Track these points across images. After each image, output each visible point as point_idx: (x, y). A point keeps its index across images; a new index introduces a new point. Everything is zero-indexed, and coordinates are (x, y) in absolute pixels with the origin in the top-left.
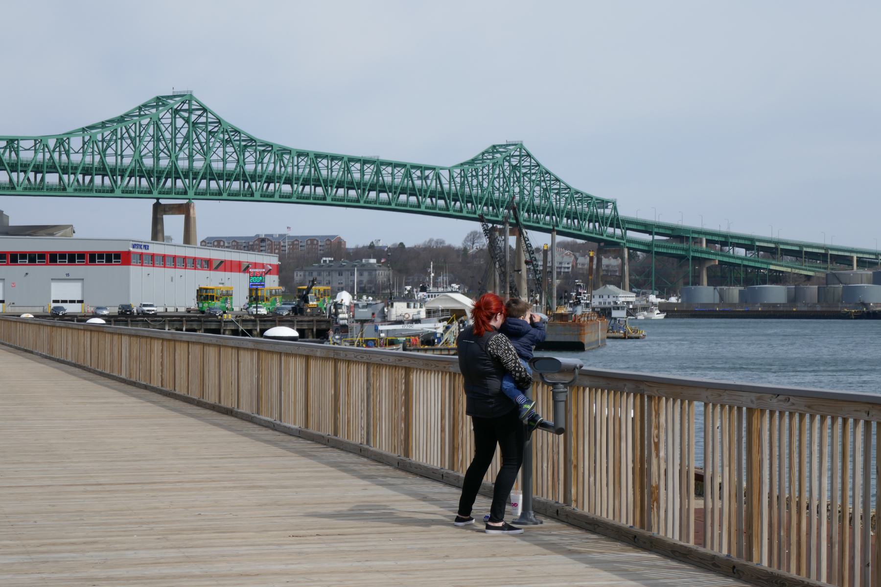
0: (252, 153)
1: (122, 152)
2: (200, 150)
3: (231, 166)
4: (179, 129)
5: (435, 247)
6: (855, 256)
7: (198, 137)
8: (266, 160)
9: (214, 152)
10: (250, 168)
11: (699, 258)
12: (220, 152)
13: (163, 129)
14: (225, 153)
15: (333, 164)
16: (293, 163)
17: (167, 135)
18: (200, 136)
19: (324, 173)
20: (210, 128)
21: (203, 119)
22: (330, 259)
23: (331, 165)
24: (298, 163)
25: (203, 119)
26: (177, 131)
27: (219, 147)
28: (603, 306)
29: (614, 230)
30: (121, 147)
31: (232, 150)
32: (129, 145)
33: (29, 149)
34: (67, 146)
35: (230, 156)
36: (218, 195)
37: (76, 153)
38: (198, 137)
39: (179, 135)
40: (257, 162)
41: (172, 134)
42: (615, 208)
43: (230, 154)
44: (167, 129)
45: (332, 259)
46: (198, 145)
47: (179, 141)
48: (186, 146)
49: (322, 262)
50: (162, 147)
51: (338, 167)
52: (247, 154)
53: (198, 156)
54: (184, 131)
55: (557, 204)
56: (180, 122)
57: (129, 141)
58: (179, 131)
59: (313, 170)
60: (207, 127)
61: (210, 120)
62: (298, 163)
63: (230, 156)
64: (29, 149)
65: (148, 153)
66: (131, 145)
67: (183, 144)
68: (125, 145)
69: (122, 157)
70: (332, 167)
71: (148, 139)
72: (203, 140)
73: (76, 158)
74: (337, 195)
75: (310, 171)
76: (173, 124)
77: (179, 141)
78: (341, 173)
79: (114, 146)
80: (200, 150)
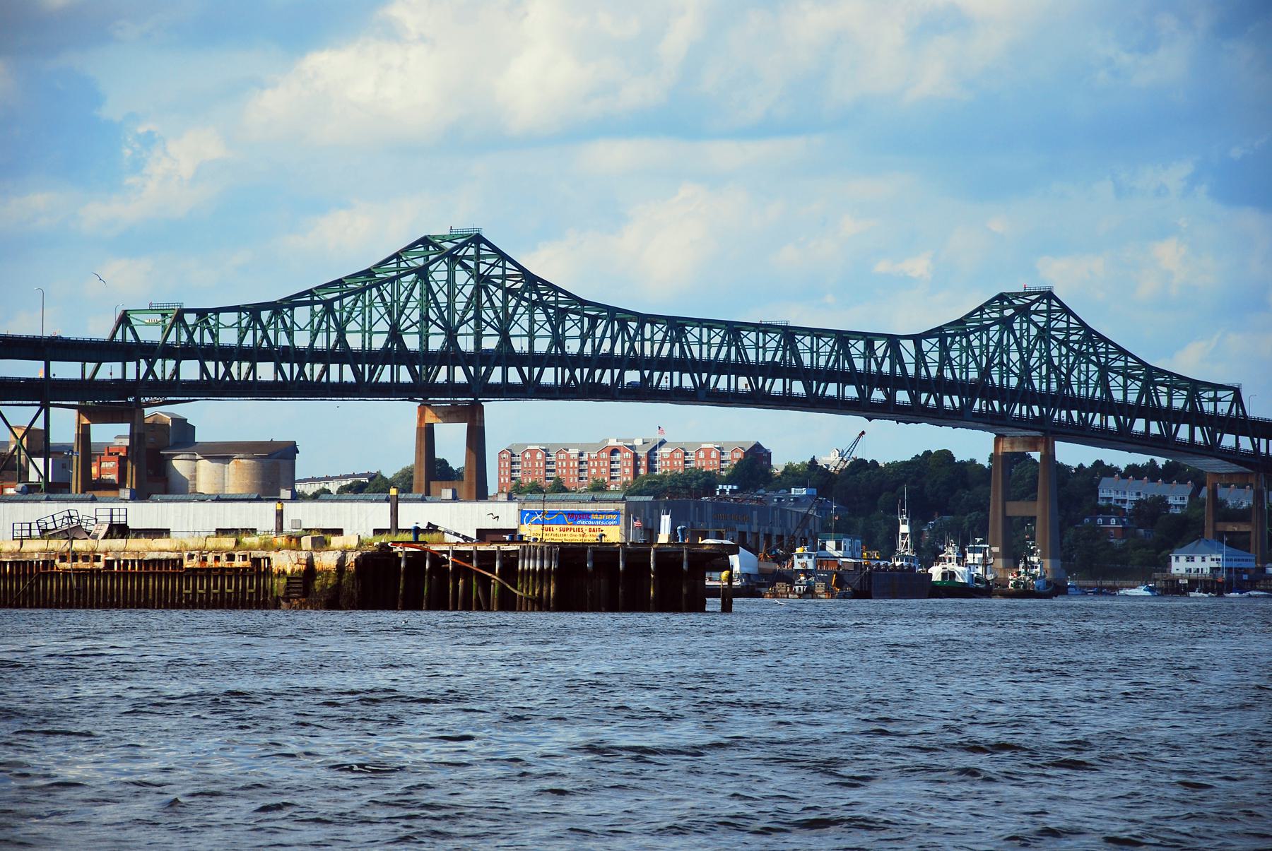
0: (576, 322)
1: (371, 326)
2: (492, 320)
3: (542, 346)
4: (460, 287)
5: (681, 471)
6: (73, 495)
7: (490, 300)
8: (599, 332)
9: (516, 322)
10: (572, 347)
11: (641, 495)
12: (524, 321)
13: (435, 289)
14: (532, 321)
15: (768, 339)
16: (643, 335)
17: (442, 298)
18: (494, 297)
19: (806, 359)
20: (508, 284)
21: (498, 271)
22: (730, 487)
23: (818, 345)
24: (709, 341)
25: (498, 271)
26: (457, 291)
27: (524, 313)
28: (1193, 575)
29: (1237, 440)
30: (370, 317)
31: (543, 317)
32: (382, 317)
33: (231, 327)
34: (288, 321)
35: (542, 327)
36: (531, 390)
37: (301, 330)
38: (490, 300)
39: (460, 298)
40: (583, 338)
41: (448, 296)
42: (1238, 399)
43: (541, 323)
44: (441, 289)
45: (735, 487)
46: (491, 313)
47: (460, 307)
48: (471, 314)
49: (718, 493)
50: (433, 316)
51: (829, 349)
52: (568, 324)
53: (489, 330)
54: (468, 290)
55: (961, 374)
56: (461, 276)
57: (383, 310)
58: (460, 291)
59: (733, 349)
60: (504, 282)
61: (508, 272)
62: (709, 341)
63: (542, 327)
64: (231, 327)
65: (411, 326)
66: (386, 316)
67: (465, 313)
68: (375, 316)
69: (371, 333)
70: (818, 349)
71: (414, 305)
72: (498, 304)
73: (302, 340)
74: (773, 390)
75: (729, 351)
76: (451, 281)
77: (460, 307)
78: (780, 354)
79: (359, 319)
80: (492, 320)
